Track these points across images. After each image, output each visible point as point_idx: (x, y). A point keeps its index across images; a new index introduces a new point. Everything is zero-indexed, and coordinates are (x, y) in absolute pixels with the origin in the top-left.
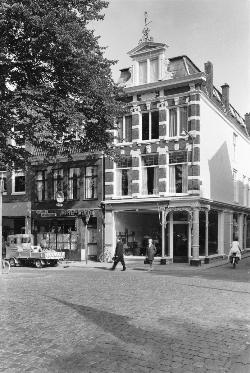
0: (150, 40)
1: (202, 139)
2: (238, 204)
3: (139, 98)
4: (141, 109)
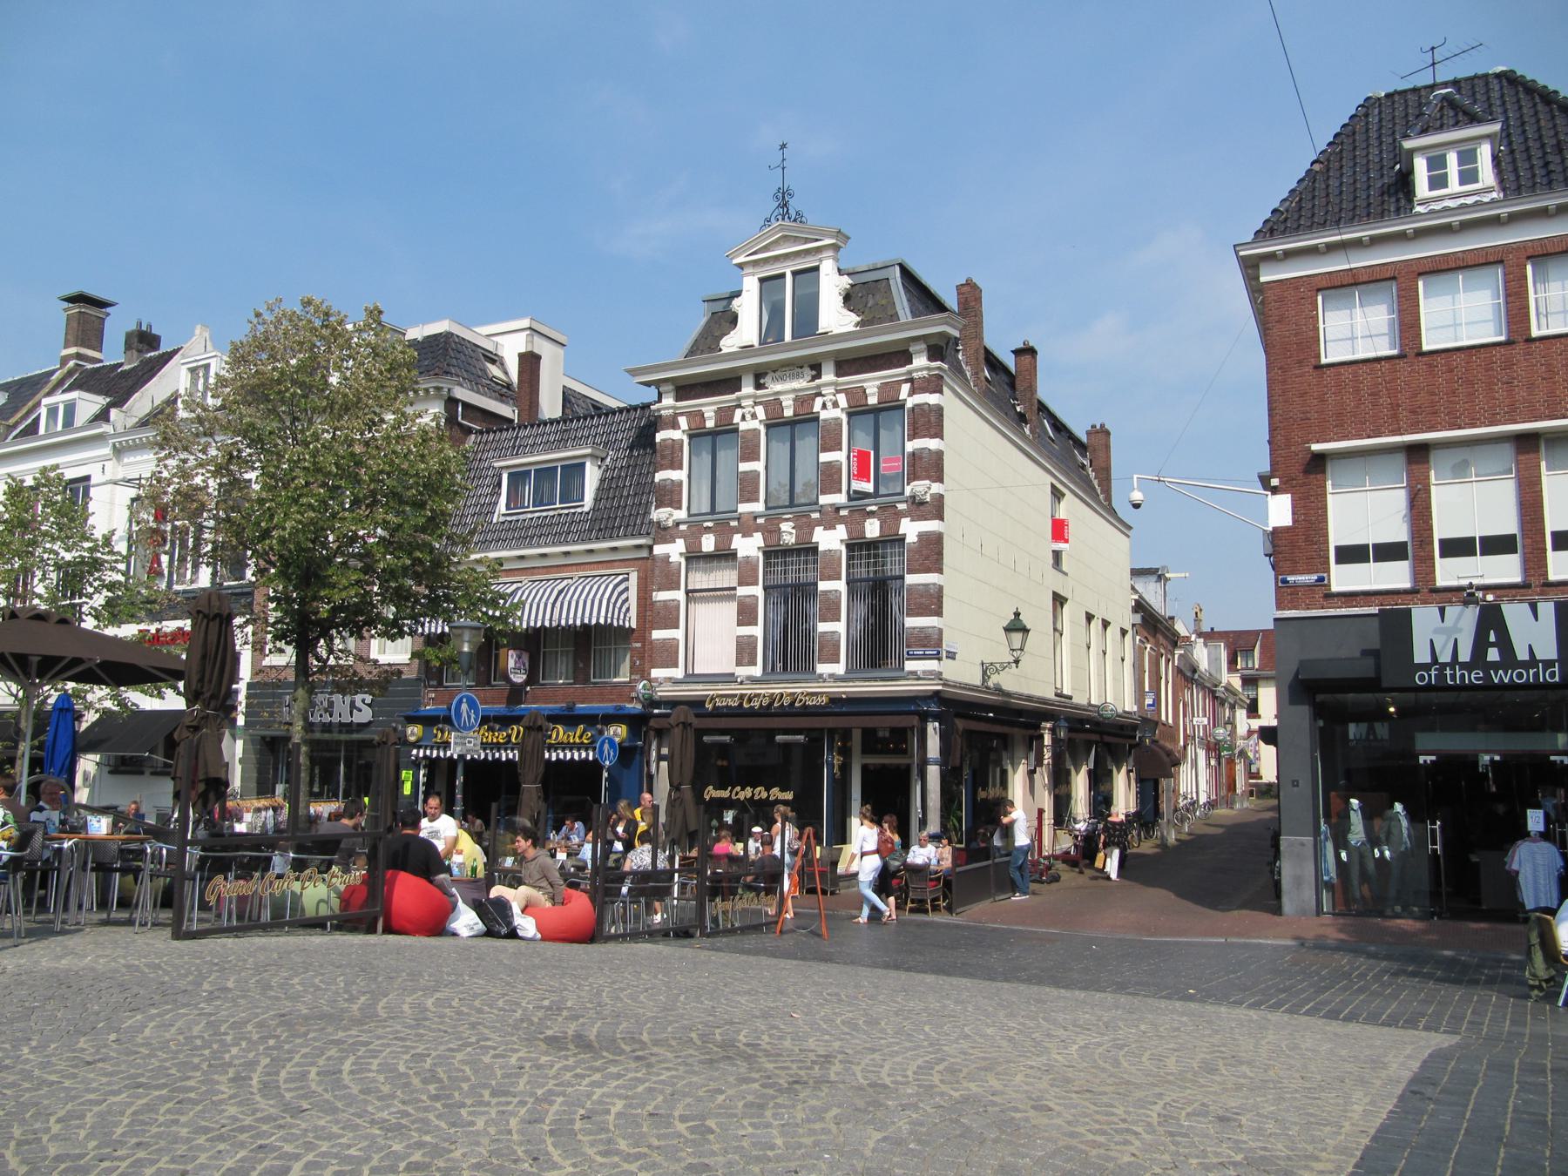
0: (795, 220)
1: (951, 553)
2: (1041, 812)
3: (762, 381)
4: (766, 414)
